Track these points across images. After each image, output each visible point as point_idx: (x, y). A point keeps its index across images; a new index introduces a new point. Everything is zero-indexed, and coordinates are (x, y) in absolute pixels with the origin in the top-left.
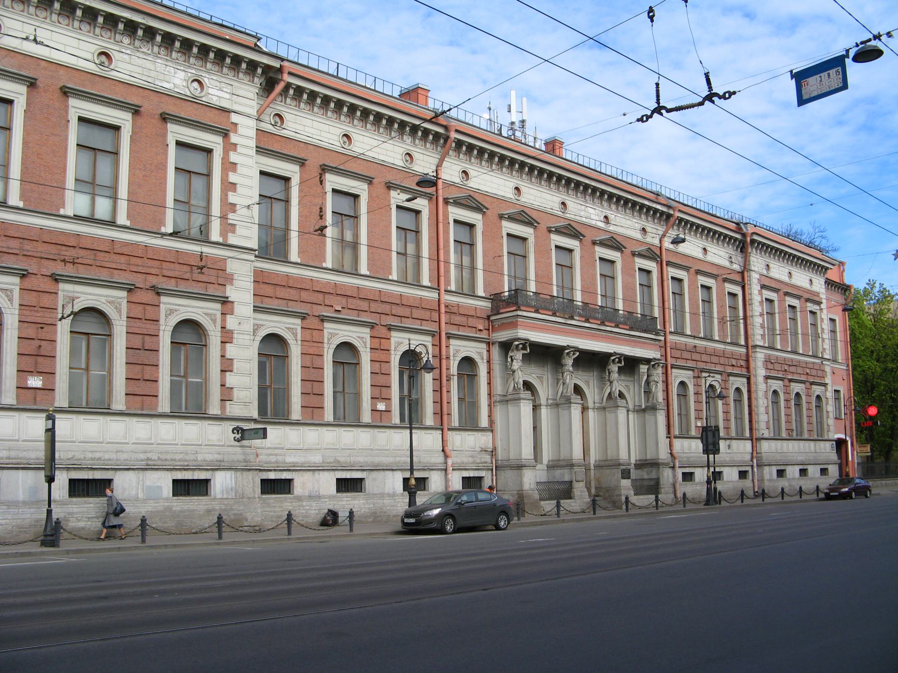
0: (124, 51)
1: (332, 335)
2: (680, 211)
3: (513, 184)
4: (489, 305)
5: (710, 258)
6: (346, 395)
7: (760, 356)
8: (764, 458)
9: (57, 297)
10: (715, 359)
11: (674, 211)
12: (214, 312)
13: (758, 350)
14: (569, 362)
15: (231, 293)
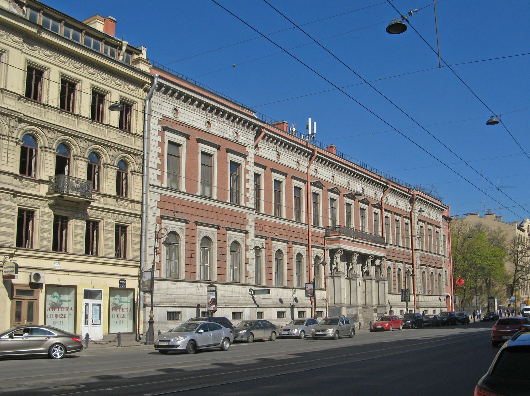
0: (214, 121)
1: (230, 237)
2: (392, 186)
4: (324, 231)
5: (213, 130)
7: (417, 255)
8: (420, 304)
10: (400, 256)
11: (389, 185)
12: (183, 227)
13: (418, 251)
14: (355, 258)
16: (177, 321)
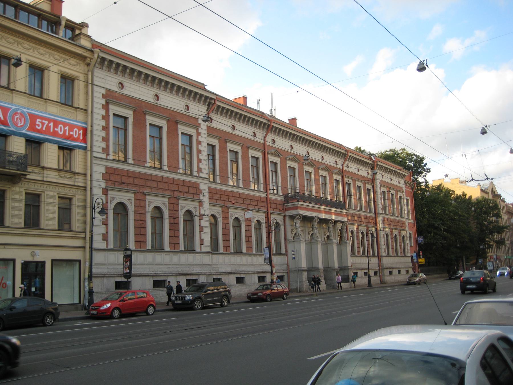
1: (151, 203)
3: (306, 149)
6: (237, 241)
7: (380, 220)
9: (146, 202)
15: (201, 197)
16: (164, 288)
